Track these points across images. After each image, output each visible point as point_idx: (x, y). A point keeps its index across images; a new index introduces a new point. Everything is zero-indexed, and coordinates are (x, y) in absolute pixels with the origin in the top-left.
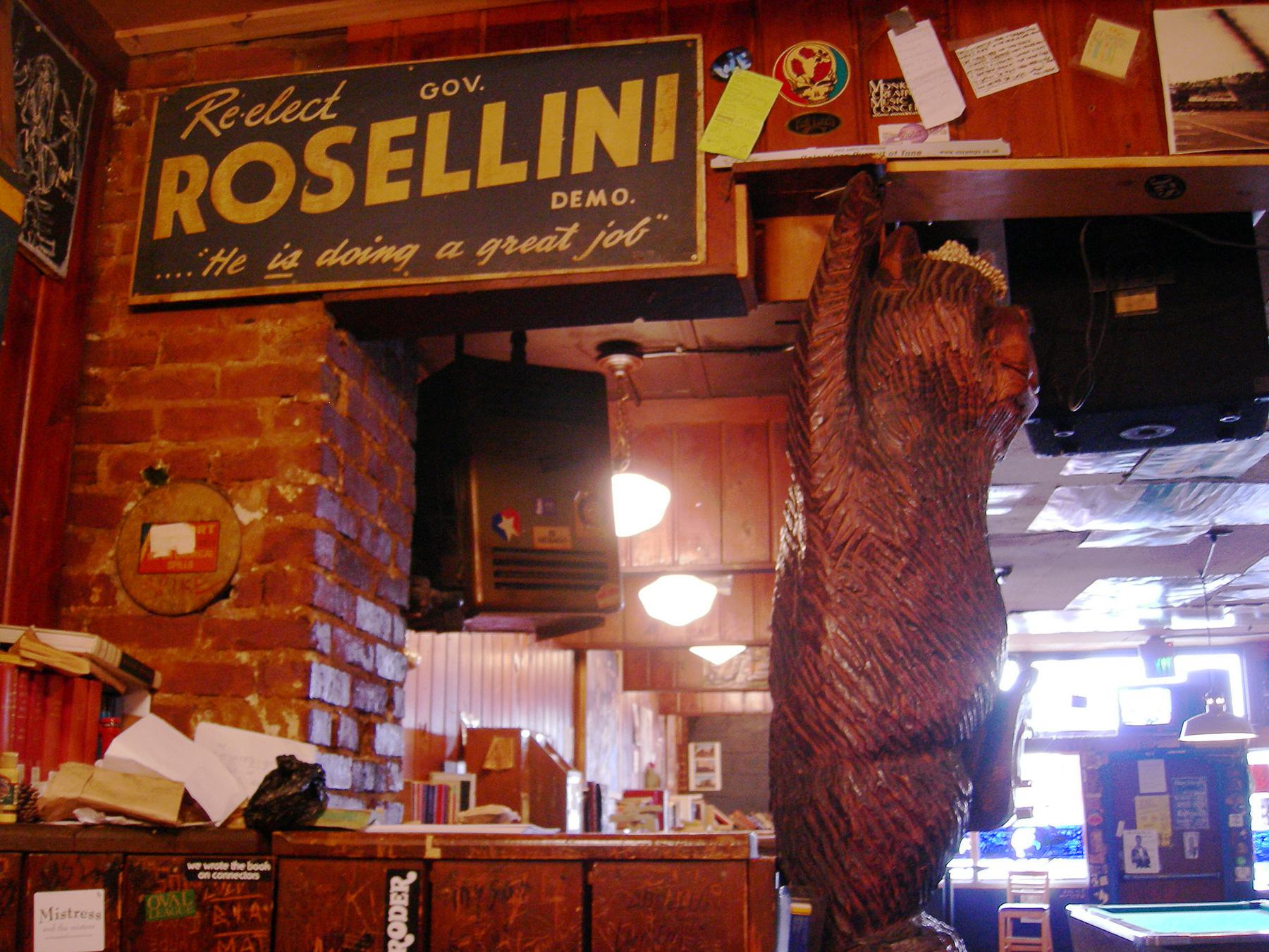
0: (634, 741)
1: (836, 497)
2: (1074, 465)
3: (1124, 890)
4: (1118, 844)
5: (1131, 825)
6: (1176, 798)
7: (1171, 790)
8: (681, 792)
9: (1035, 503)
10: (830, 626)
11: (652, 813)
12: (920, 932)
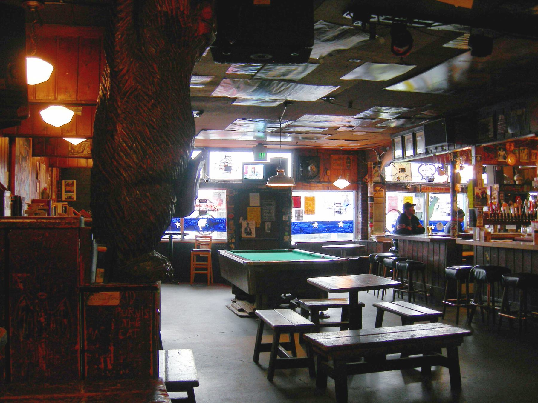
0: (37, 178)
1: (124, 71)
2: (234, 69)
3: (238, 242)
4: (240, 226)
5: (245, 218)
6: (264, 208)
7: (261, 205)
8: (58, 201)
9: (215, 84)
10: (119, 128)
11: (44, 210)
12: (154, 259)
